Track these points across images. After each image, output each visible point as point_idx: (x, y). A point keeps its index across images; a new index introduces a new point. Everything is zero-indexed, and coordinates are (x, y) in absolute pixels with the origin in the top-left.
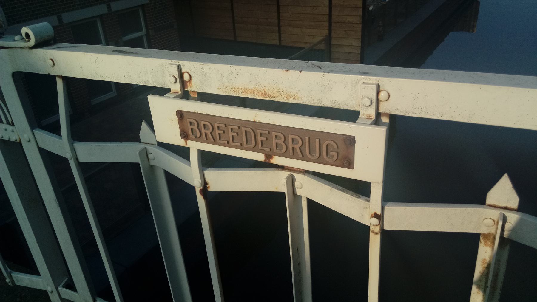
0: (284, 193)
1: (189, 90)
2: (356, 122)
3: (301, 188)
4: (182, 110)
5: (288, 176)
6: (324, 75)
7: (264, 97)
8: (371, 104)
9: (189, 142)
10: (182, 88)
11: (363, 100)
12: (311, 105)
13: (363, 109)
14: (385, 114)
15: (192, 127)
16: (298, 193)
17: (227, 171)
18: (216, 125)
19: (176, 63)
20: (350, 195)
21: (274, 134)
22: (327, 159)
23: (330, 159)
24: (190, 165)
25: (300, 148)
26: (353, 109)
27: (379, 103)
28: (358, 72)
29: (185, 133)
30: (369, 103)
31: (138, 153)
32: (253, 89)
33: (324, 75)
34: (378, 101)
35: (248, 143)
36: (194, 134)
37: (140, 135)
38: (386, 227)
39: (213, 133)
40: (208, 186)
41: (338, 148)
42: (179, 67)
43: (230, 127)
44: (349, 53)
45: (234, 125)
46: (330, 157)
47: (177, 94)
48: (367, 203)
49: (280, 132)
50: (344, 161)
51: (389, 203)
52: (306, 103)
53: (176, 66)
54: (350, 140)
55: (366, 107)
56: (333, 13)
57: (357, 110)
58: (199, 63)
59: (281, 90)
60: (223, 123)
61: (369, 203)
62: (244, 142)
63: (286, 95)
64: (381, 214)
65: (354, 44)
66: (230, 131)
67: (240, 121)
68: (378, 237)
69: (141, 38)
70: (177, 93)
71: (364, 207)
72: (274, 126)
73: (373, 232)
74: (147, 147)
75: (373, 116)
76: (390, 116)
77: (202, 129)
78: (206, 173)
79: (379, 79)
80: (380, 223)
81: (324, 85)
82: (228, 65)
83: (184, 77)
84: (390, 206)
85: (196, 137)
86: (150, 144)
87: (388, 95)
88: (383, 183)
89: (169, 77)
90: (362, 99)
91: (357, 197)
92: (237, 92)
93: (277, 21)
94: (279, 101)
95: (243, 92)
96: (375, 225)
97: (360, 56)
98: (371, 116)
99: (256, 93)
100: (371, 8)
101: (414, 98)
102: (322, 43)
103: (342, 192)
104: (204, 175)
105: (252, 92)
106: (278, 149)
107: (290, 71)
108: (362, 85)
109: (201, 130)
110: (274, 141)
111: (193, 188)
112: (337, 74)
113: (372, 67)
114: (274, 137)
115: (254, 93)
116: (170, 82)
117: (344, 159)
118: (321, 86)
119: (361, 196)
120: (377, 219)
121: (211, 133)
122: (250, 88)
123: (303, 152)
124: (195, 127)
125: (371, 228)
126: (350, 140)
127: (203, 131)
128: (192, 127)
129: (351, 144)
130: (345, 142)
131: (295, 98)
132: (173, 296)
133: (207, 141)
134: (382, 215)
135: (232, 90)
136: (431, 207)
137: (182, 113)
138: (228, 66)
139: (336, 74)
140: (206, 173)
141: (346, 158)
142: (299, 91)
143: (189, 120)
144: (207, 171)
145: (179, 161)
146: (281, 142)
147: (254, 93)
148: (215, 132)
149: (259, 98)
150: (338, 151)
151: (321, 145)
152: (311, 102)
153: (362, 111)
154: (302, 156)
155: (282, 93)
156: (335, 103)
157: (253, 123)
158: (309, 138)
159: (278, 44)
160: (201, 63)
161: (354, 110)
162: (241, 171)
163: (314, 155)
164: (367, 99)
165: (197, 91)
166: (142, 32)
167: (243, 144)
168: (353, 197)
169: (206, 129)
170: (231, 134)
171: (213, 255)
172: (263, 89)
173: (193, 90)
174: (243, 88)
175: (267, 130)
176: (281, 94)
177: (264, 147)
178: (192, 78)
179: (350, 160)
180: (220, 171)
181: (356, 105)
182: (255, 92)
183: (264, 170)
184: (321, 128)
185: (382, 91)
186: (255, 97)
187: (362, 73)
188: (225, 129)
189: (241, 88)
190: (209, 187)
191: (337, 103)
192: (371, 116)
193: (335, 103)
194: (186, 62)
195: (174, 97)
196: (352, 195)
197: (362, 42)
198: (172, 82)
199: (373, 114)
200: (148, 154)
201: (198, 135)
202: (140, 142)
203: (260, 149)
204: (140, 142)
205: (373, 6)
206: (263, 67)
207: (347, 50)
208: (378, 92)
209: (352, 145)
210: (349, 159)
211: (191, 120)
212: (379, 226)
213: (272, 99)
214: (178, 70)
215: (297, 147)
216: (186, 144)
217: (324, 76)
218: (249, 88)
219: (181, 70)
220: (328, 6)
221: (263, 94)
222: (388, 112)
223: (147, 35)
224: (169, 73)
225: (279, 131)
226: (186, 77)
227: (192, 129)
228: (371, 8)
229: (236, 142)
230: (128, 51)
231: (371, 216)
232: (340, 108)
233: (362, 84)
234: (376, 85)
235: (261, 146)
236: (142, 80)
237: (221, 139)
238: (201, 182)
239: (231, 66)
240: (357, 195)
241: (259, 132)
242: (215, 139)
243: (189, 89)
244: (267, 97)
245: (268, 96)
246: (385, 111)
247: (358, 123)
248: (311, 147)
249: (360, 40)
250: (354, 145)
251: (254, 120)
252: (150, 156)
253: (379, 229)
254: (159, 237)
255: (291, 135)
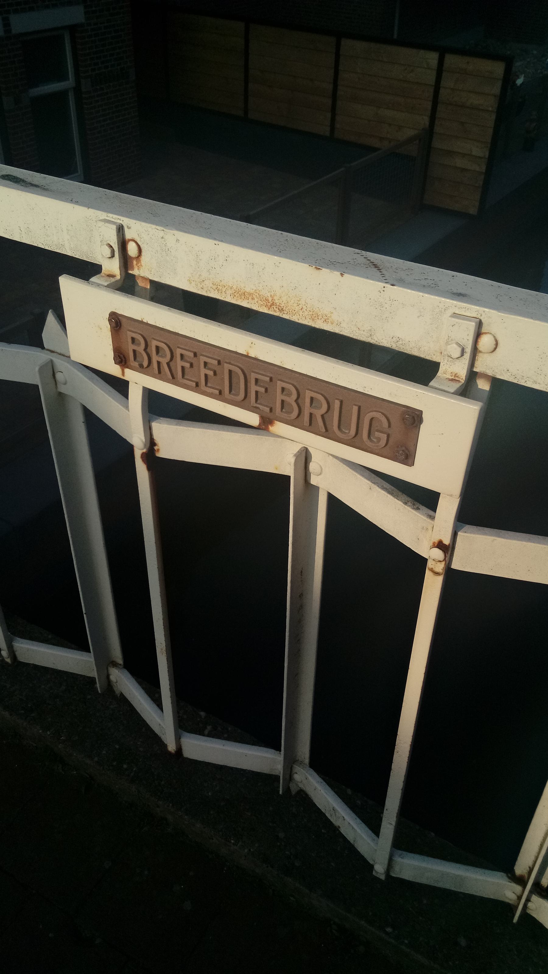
0: (289, 477)
1: (136, 274)
2: (432, 383)
3: (320, 474)
4: (120, 312)
5: (298, 452)
6: (384, 287)
7: (271, 309)
8: (462, 355)
9: (127, 371)
10: (123, 270)
11: (449, 347)
12: (354, 337)
13: (446, 361)
14: (485, 376)
15: (135, 348)
16: (314, 481)
17: (193, 427)
18: (178, 352)
19: (115, 221)
20: (402, 502)
21: (280, 385)
22: (369, 444)
23: (374, 445)
24: (127, 407)
25: (322, 416)
26: (428, 358)
27: (477, 354)
28: (448, 291)
29: (122, 356)
30: (457, 353)
31: (37, 369)
32: (252, 291)
33: (384, 287)
34: (475, 350)
35: (233, 392)
36: (138, 359)
37: (43, 335)
38: (456, 565)
39: (171, 364)
40: (156, 448)
41: (390, 426)
42: (120, 229)
43: (203, 359)
44: (463, 170)
45: (211, 356)
46: (375, 440)
47: (112, 280)
48: (429, 520)
49: (292, 382)
50: (398, 452)
51: (467, 527)
52: (346, 332)
53: (114, 227)
54: (413, 417)
55: (451, 359)
56: (443, 83)
57: (434, 360)
58: (157, 227)
59: (302, 302)
60: (191, 350)
61: (433, 522)
62: (225, 390)
63: (311, 313)
64: (449, 545)
65: (474, 153)
66: (203, 365)
67: (222, 351)
68: (440, 580)
69: (62, 95)
70: (113, 276)
71: (423, 527)
72: (281, 370)
73: (432, 570)
74: (54, 359)
75: (461, 378)
76: (493, 380)
77: (153, 354)
78: (155, 425)
79: (484, 312)
80: (446, 558)
81: (382, 306)
82: (211, 241)
83: (128, 249)
84: (468, 533)
85: (141, 366)
86: (60, 354)
87: (495, 343)
88: (461, 495)
89: (102, 245)
90: (447, 343)
91: (414, 509)
92: (223, 292)
93: (331, 87)
94: (297, 321)
95: (233, 295)
96: (437, 561)
97: (483, 177)
98: (457, 377)
99: (256, 300)
100: (519, 82)
101: (541, 356)
102: (415, 142)
103: (389, 496)
104: (150, 428)
105: (250, 298)
106: (284, 410)
107: (323, 269)
108: (450, 318)
109: (151, 356)
110: (279, 397)
111: (130, 448)
112: (409, 291)
113: (476, 281)
114: (279, 390)
115: (254, 299)
116: (102, 255)
117: (398, 447)
118: (377, 307)
119: (421, 507)
120: (443, 551)
121: (168, 364)
122: (248, 290)
123: (327, 423)
124: (141, 349)
125: (430, 564)
126: (413, 417)
127: (155, 358)
128: (135, 348)
129: (415, 425)
130: (403, 420)
131: (327, 320)
132: (84, 612)
133: (159, 375)
134: (451, 546)
135: (215, 287)
136: (539, 543)
137: (118, 319)
138: (211, 242)
139: (405, 290)
140: (155, 425)
141: (401, 447)
142: (336, 309)
143: (130, 334)
144: (157, 423)
145: (109, 396)
146: (291, 400)
147: (254, 299)
148: (176, 362)
149: (261, 310)
150: (390, 433)
151: (361, 417)
152: (354, 332)
153: (444, 365)
154: (325, 431)
155: (304, 307)
156: (397, 341)
157: (244, 358)
158: (341, 402)
159: (328, 134)
160: (162, 228)
161: (430, 359)
162: (217, 431)
163: (347, 431)
164: (455, 345)
165: (150, 278)
166: (67, 82)
167: (223, 392)
168: (406, 507)
169: (160, 354)
170: (203, 371)
171: (156, 563)
172: (271, 295)
173: (142, 275)
174: (235, 287)
175: (269, 375)
176: (301, 309)
177: (259, 404)
178: (143, 253)
179: (409, 451)
180: (180, 425)
181: (436, 351)
182: (256, 299)
183: (258, 435)
184: (365, 387)
185: (486, 333)
186: (255, 307)
187: (454, 294)
188: (194, 361)
189: (231, 286)
190: (158, 450)
191: (401, 342)
192: (457, 377)
193: (397, 341)
194: (134, 221)
195: (108, 286)
196: (406, 503)
197: (492, 151)
198: (104, 255)
199: (463, 373)
200: (55, 372)
201: (145, 364)
202: (43, 348)
203: (252, 407)
204: (43, 348)
205: (524, 76)
206: (274, 254)
207: (459, 162)
208: (478, 335)
209: (416, 426)
210: (407, 449)
211: (134, 335)
212: (443, 563)
213: (285, 316)
214: (117, 235)
215: (318, 413)
216: (123, 374)
217: (384, 289)
218: (245, 289)
219: (123, 235)
220: (434, 84)
221: (269, 304)
222: (490, 373)
223: (77, 89)
224: (101, 238)
225: (290, 381)
226: (132, 249)
227: (134, 351)
228: (519, 82)
229: (210, 387)
230: (29, 180)
231: (431, 544)
232: (406, 352)
233: (451, 316)
234: (476, 323)
235: (254, 400)
236: (51, 242)
237: (186, 377)
238: (144, 440)
239: (217, 242)
240: (414, 505)
241: (253, 377)
242: (175, 376)
243: (135, 272)
244: (275, 311)
245: (279, 309)
246: (484, 370)
247: (432, 387)
248: (342, 419)
249: (489, 146)
250: (418, 427)
251: (248, 353)
252: (59, 376)
253: (443, 568)
254: (66, 516)
255: (309, 391)
